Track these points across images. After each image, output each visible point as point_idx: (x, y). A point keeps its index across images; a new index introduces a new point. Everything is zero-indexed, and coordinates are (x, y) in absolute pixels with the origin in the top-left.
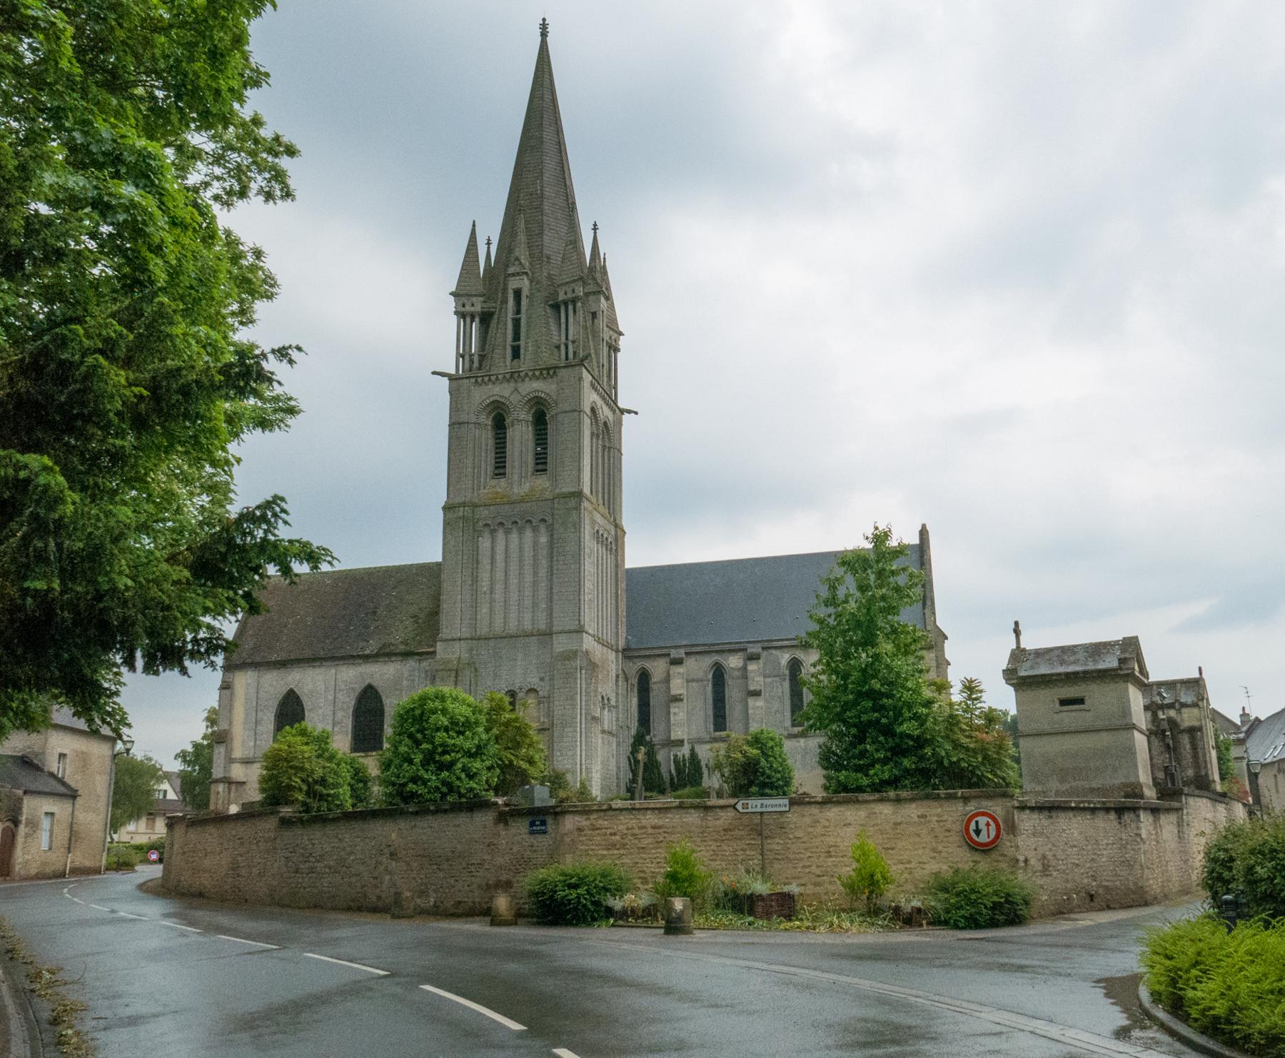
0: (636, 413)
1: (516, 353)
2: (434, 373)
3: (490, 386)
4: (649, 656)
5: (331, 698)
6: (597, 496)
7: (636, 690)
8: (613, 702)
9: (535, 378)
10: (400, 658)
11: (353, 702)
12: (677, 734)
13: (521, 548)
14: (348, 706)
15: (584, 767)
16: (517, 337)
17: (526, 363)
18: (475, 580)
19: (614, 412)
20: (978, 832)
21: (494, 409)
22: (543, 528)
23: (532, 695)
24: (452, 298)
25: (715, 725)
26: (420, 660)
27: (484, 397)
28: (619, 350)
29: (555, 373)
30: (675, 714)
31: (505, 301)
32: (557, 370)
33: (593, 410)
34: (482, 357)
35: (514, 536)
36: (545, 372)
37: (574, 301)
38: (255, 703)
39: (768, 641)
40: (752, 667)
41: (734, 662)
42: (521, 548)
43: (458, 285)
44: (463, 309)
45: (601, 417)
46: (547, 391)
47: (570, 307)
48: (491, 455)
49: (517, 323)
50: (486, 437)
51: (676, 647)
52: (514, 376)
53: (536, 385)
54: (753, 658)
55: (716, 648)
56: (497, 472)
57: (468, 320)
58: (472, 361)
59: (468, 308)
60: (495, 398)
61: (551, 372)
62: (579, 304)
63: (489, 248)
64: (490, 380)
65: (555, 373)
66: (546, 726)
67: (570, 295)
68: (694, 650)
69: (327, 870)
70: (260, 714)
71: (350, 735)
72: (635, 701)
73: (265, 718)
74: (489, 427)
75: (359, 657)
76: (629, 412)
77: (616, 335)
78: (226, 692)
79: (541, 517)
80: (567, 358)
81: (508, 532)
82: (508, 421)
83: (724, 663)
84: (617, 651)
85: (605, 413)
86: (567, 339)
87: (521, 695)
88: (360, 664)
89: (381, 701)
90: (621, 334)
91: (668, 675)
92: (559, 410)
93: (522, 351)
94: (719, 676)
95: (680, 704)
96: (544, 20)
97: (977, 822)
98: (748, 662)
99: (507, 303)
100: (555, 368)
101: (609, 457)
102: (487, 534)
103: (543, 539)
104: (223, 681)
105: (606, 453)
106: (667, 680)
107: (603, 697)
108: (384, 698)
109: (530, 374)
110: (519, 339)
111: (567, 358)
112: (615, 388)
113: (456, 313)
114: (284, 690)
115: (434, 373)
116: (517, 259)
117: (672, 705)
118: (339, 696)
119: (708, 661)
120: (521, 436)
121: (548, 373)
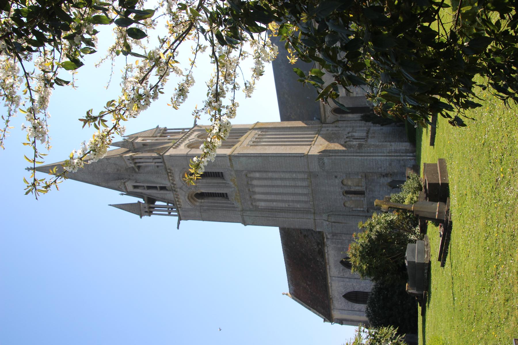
2: (178, 228)
5: (347, 280)
7: (344, 115)
13: (261, 186)
15: (388, 154)
16: (155, 188)
24: (143, 217)
28: (166, 128)
30: (357, 94)
36: (170, 174)
42: (261, 186)
43: (139, 215)
48: (216, 198)
50: (206, 202)
60: (187, 200)
77: (158, 130)
80: (161, 162)
87: (346, 189)
90: (158, 127)
93: (162, 185)
96: (26, 169)
103: (257, 175)
107: (347, 138)
111: (161, 162)
112: (184, 129)
115: (178, 228)
118: (346, 276)
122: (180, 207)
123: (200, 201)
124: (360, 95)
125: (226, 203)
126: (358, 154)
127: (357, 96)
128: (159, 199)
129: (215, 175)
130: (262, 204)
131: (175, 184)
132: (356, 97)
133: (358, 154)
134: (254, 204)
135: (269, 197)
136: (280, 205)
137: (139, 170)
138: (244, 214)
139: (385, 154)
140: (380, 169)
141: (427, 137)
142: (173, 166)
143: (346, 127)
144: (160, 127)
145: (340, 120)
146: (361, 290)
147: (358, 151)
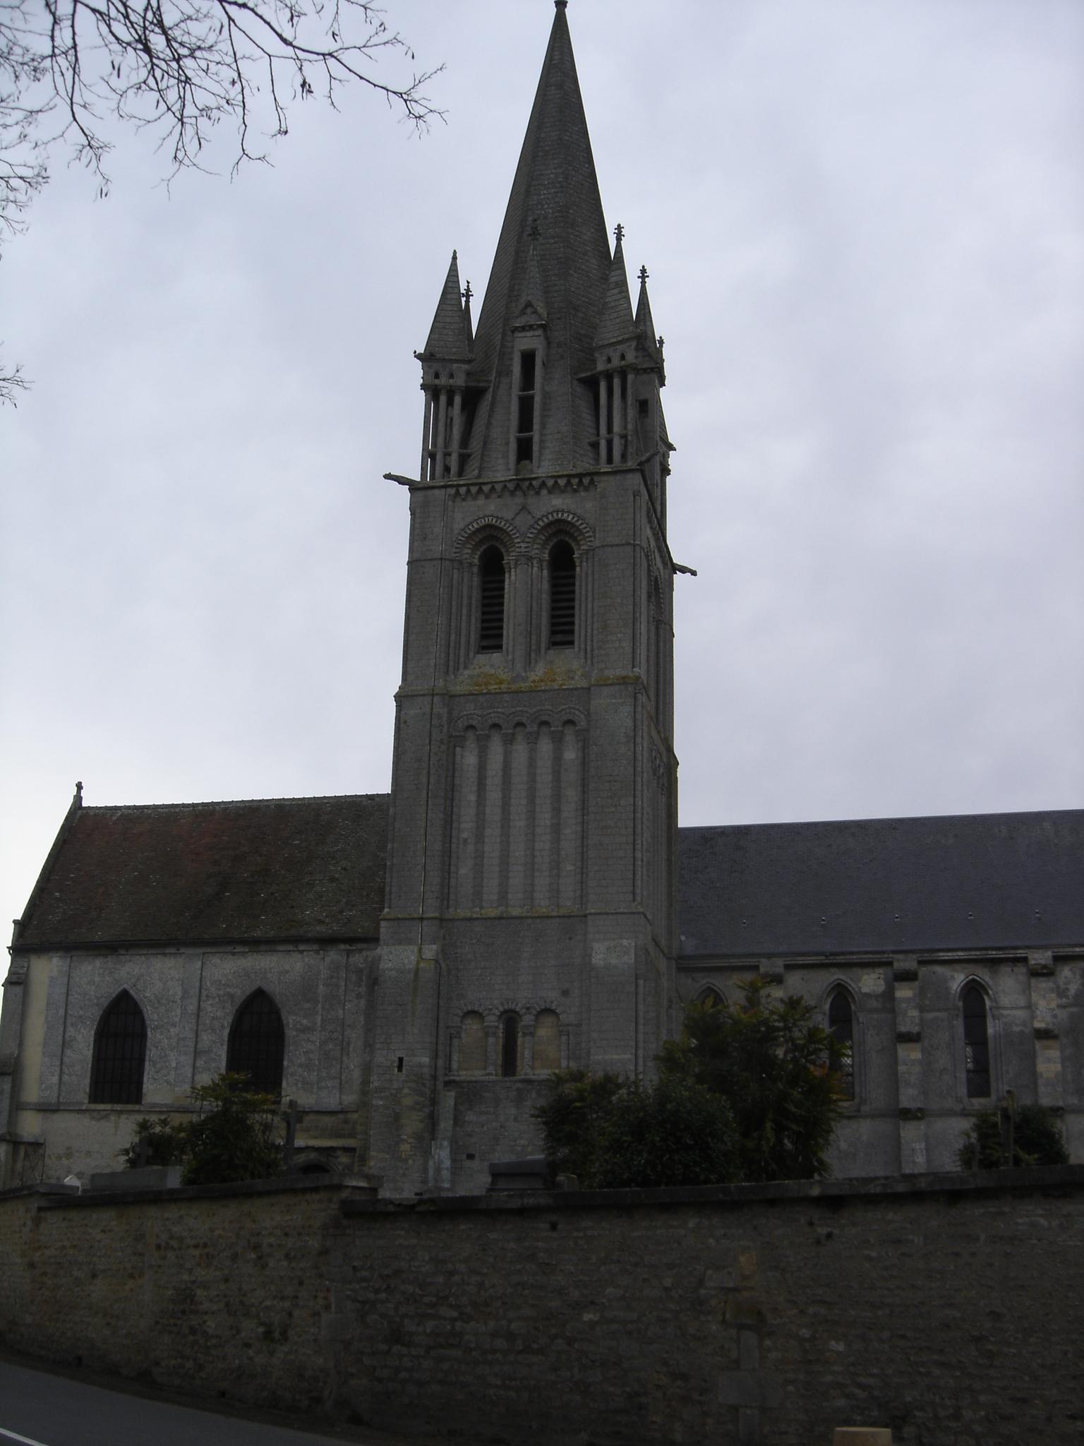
0: (694, 573)
1: (524, 451)
2: (388, 477)
3: (481, 501)
5: (192, 1008)
9: (555, 489)
10: (316, 947)
11: (230, 1019)
13: (532, 764)
14: (223, 1026)
16: (525, 423)
17: (544, 466)
18: (449, 821)
21: (481, 542)
22: (570, 737)
23: (549, 1020)
26: (348, 953)
27: (468, 520)
29: (592, 482)
31: (505, 372)
35: (520, 751)
38: (62, 1012)
39: (928, 951)
40: (904, 992)
41: (870, 983)
42: (532, 764)
44: (437, 381)
46: (579, 512)
47: (617, 382)
50: (471, 584)
51: (769, 956)
52: (522, 486)
53: (558, 502)
54: (907, 977)
55: (840, 959)
56: (485, 643)
59: (443, 381)
61: (586, 481)
64: (480, 490)
65: (592, 482)
67: (616, 362)
68: (801, 960)
69: (501, 1343)
70: (71, 1032)
73: (79, 1037)
74: (475, 569)
75: (244, 942)
76: (684, 570)
78: (18, 989)
79: (565, 718)
81: (509, 741)
82: (508, 559)
83: (853, 986)
86: (610, 429)
87: (527, 1020)
88: (243, 954)
89: (279, 1019)
90: (671, 448)
92: (597, 543)
93: (535, 448)
100: (591, 474)
102: (471, 743)
103: (570, 754)
104: (12, 972)
108: (284, 1015)
109: (550, 483)
110: (530, 429)
113: (423, 387)
114: (115, 991)
115: (388, 477)
118: (207, 1006)
121: (581, 482)
122: (458, 493)
130: (469, 759)
131: (538, 493)
138: (436, 699)
146: (151, 1053)
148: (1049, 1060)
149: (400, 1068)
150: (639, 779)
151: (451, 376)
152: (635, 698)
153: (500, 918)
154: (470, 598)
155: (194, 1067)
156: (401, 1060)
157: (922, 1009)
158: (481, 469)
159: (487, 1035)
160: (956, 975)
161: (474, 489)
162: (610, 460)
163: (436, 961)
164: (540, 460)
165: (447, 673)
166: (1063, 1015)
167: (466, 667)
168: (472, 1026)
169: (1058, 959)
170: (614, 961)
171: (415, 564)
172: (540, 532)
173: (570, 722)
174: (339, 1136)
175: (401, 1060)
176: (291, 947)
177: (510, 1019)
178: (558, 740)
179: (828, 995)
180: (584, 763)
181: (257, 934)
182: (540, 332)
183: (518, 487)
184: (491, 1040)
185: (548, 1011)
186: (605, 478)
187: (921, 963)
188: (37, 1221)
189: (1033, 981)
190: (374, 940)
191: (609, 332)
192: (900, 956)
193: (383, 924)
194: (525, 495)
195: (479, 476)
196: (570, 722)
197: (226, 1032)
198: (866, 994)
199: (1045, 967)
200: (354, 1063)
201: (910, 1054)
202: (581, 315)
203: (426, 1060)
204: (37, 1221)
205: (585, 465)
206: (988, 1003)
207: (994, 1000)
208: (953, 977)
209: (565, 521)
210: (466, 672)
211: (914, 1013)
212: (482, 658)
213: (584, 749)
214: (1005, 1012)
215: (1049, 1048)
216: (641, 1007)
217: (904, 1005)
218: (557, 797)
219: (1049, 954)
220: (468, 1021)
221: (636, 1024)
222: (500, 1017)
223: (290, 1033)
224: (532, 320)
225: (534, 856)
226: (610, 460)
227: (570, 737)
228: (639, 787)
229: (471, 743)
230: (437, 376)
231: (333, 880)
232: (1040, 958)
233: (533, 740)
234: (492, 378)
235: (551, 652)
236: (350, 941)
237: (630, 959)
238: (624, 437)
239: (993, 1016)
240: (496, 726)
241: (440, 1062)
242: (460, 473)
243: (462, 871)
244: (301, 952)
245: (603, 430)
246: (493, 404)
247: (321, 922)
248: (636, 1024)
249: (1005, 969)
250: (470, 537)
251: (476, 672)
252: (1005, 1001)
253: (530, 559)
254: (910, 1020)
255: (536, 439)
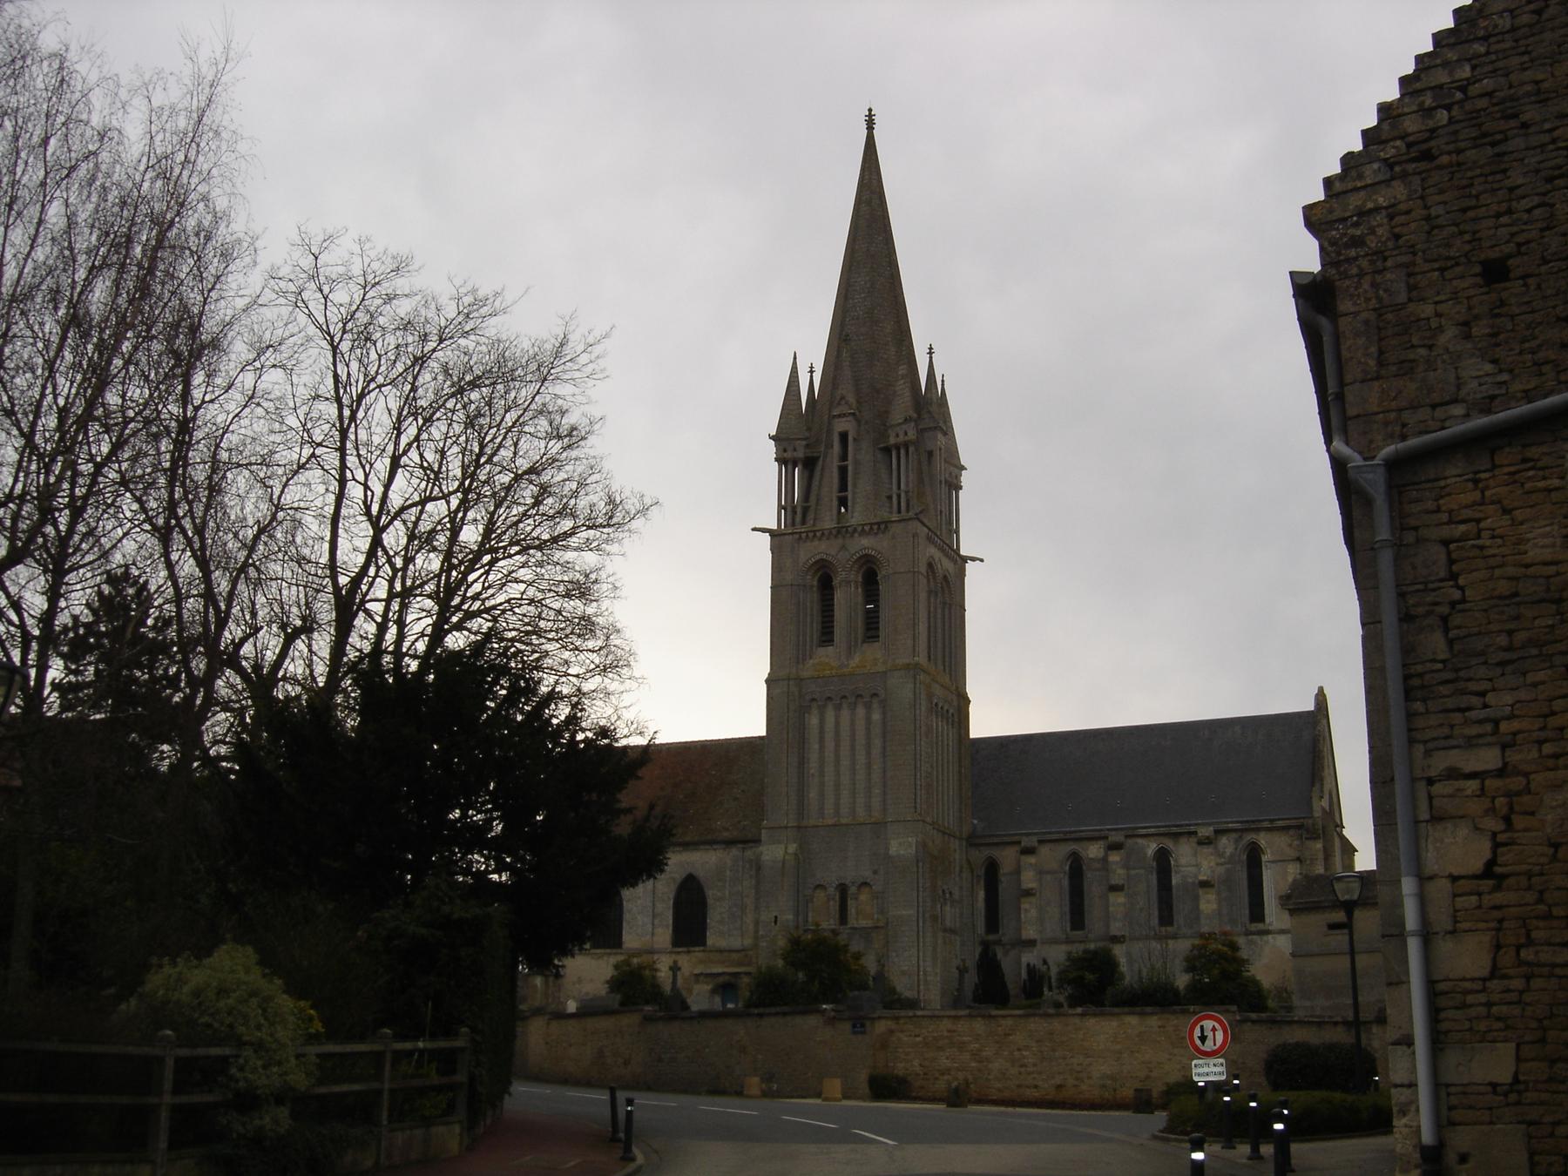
0: (982, 560)
2: (754, 529)
3: (816, 543)
4: (997, 844)
6: (936, 664)
7: (982, 883)
8: (956, 896)
9: (863, 533)
10: (723, 846)
12: (1029, 932)
14: (669, 898)
15: (921, 969)
16: (843, 486)
17: (856, 517)
18: (802, 762)
19: (955, 562)
20: (1203, 1038)
21: (818, 570)
23: (867, 889)
25: (1072, 923)
26: (744, 848)
29: (886, 527)
30: (1026, 910)
32: (889, 525)
33: (930, 566)
34: (805, 510)
35: (845, 714)
37: (906, 445)
40: (1114, 857)
41: (1094, 851)
44: (785, 455)
45: (940, 572)
49: (843, 471)
50: (812, 599)
51: (1028, 835)
52: (842, 531)
55: (1073, 836)
56: (824, 639)
57: (790, 467)
58: (794, 512)
61: (883, 526)
62: (911, 449)
63: (811, 377)
65: (886, 527)
66: (881, 924)
67: (902, 438)
71: (671, 928)
72: (981, 894)
74: (815, 589)
76: (973, 559)
81: (838, 708)
82: (835, 582)
83: (1083, 854)
84: (961, 839)
85: (948, 565)
86: (899, 488)
87: (853, 890)
88: (680, 852)
90: (963, 468)
91: (1019, 867)
94: (1076, 869)
95: (1033, 899)
96: (870, 110)
97: (1202, 1027)
98: (1109, 852)
99: (832, 446)
100: (886, 522)
101: (950, 613)
102: (815, 711)
103: (876, 716)
105: (947, 611)
106: (1018, 871)
107: (943, 891)
108: (706, 890)
113: (776, 460)
115: (754, 529)
116: (843, 398)
117: (1023, 900)
119: (1066, 849)
120: (847, 599)
122: (800, 538)
123: (815, 583)
124: (1023, 916)
125: (812, 641)
126: (921, 915)
127: (1022, 911)
128: (815, 483)
129: (872, 615)
130: (814, 721)
131: (852, 536)
132: (1020, 909)
133: (921, 915)
134: (814, 705)
135: (829, 736)
136: (813, 757)
137: (881, 449)
138: (791, 683)
139: (921, 963)
140: (894, 954)
141: (1534, 717)
142: (893, 537)
143: (961, 888)
144: (963, 472)
145: (973, 876)
146: (627, 916)
147: (927, 915)
148: (1208, 902)
149: (776, 922)
150: (918, 733)
151: (795, 450)
152: (915, 679)
153: (835, 825)
154: (812, 609)
155: (653, 924)
156: (776, 917)
157: (1127, 867)
158: (815, 519)
159: (829, 900)
160: (1151, 844)
161: (811, 535)
162: (899, 512)
163: (796, 854)
164: (853, 512)
165: (798, 663)
166: (1221, 870)
167: (811, 658)
168: (820, 894)
169: (1218, 832)
170: (902, 852)
171: (776, 588)
172: (854, 562)
173: (875, 695)
174: (740, 964)
175: (776, 917)
176: (708, 847)
177: (843, 889)
178: (868, 707)
179: (1068, 860)
180: (884, 723)
181: (688, 839)
182: (850, 418)
183: (839, 532)
184: (831, 903)
185: (865, 884)
186: (895, 525)
187: (1127, 837)
188: (548, 1024)
189: (1199, 848)
190: (757, 841)
191: (901, 408)
192: (1113, 833)
193: (763, 831)
194: (844, 537)
195: (814, 525)
196: (875, 695)
197: (672, 902)
198: (1091, 859)
199: (1208, 838)
200: (749, 919)
201: (1118, 899)
202: (882, 396)
203: (791, 917)
204: (548, 1024)
205: (884, 514)
206: (1172, 862)
207: (1176, 861)
208: (1148, 846)
209: (870, 555)
210: (811, 661)
211: (1121, 871)
212: (821, 651)
213: (884, 713)
214: (1183, 869)
215: (1208, 893)
216: (921, 881)
217: (1114, 867)
218: (868, 746)
219: (1212, 828)
220: (818, 891)
221: (918, 891)
222: (836, 888)
223: (710, 901)
224: (846, 410)
225: (854, 784)
226: (899, 512)
227: (875, 705)
228: (918, 738)
229: (815, 711)
230: (785, 451)
231: (736, 799)
232: (1206, 831)
233: (853, 707)
234: (822, 449)
235: (865, 645)
236: (745, 842)
237: (912, 851)
238: (907, 492)
239: (1176, 872)
240: (829, 698)
241: (800, 918)
242: (804, 522)
243: (811, 795)
244: (715, 850)
245: (895, 487)
246: (823, 469)
247: (727, 830)
248: (918, 891)
249: (1183, 840)
250: (809, 569)
251: (816, 661)
252: (1183, 861)
253: (849, 582)
254: (1118, 875)
255: (850, 497)
